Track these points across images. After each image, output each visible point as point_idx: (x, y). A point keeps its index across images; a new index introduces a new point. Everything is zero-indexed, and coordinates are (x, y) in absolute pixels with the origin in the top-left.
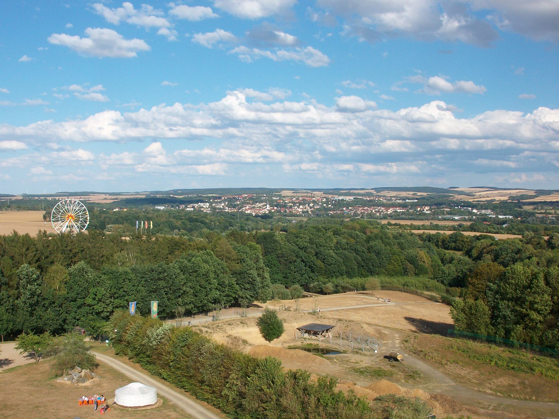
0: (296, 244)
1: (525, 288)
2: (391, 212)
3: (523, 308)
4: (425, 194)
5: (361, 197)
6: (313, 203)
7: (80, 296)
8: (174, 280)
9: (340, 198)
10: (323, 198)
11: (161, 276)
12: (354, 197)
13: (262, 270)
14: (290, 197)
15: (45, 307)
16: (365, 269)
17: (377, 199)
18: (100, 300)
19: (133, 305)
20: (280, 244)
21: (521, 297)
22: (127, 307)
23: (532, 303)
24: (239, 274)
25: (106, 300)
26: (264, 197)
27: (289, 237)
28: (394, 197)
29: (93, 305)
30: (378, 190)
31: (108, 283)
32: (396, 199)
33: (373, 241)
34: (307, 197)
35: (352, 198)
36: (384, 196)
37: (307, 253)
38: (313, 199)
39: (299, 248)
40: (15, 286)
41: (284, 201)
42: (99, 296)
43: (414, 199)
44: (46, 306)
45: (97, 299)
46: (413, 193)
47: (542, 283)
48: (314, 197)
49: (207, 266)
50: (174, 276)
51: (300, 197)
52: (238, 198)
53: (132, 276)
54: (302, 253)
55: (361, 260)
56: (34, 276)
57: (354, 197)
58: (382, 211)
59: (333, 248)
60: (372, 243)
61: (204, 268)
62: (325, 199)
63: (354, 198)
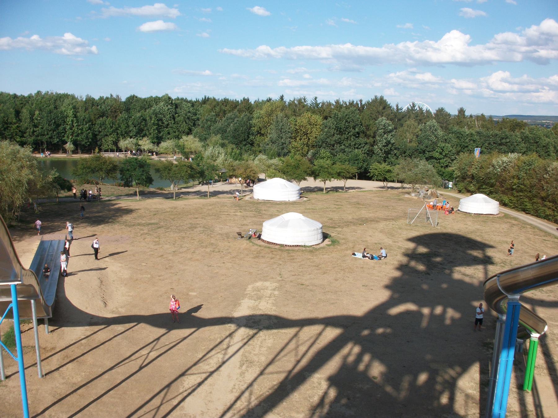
7: (428, 149)
8: (515, 147)
11: (504, 141)
15: (396, 156)
18: (446, 156)
19: (477, 151)
22: (472, 152)
40: (372, 134)
44: (397, 155)
45: (444, 154)
50: (515, 144)
56: (390, 128)
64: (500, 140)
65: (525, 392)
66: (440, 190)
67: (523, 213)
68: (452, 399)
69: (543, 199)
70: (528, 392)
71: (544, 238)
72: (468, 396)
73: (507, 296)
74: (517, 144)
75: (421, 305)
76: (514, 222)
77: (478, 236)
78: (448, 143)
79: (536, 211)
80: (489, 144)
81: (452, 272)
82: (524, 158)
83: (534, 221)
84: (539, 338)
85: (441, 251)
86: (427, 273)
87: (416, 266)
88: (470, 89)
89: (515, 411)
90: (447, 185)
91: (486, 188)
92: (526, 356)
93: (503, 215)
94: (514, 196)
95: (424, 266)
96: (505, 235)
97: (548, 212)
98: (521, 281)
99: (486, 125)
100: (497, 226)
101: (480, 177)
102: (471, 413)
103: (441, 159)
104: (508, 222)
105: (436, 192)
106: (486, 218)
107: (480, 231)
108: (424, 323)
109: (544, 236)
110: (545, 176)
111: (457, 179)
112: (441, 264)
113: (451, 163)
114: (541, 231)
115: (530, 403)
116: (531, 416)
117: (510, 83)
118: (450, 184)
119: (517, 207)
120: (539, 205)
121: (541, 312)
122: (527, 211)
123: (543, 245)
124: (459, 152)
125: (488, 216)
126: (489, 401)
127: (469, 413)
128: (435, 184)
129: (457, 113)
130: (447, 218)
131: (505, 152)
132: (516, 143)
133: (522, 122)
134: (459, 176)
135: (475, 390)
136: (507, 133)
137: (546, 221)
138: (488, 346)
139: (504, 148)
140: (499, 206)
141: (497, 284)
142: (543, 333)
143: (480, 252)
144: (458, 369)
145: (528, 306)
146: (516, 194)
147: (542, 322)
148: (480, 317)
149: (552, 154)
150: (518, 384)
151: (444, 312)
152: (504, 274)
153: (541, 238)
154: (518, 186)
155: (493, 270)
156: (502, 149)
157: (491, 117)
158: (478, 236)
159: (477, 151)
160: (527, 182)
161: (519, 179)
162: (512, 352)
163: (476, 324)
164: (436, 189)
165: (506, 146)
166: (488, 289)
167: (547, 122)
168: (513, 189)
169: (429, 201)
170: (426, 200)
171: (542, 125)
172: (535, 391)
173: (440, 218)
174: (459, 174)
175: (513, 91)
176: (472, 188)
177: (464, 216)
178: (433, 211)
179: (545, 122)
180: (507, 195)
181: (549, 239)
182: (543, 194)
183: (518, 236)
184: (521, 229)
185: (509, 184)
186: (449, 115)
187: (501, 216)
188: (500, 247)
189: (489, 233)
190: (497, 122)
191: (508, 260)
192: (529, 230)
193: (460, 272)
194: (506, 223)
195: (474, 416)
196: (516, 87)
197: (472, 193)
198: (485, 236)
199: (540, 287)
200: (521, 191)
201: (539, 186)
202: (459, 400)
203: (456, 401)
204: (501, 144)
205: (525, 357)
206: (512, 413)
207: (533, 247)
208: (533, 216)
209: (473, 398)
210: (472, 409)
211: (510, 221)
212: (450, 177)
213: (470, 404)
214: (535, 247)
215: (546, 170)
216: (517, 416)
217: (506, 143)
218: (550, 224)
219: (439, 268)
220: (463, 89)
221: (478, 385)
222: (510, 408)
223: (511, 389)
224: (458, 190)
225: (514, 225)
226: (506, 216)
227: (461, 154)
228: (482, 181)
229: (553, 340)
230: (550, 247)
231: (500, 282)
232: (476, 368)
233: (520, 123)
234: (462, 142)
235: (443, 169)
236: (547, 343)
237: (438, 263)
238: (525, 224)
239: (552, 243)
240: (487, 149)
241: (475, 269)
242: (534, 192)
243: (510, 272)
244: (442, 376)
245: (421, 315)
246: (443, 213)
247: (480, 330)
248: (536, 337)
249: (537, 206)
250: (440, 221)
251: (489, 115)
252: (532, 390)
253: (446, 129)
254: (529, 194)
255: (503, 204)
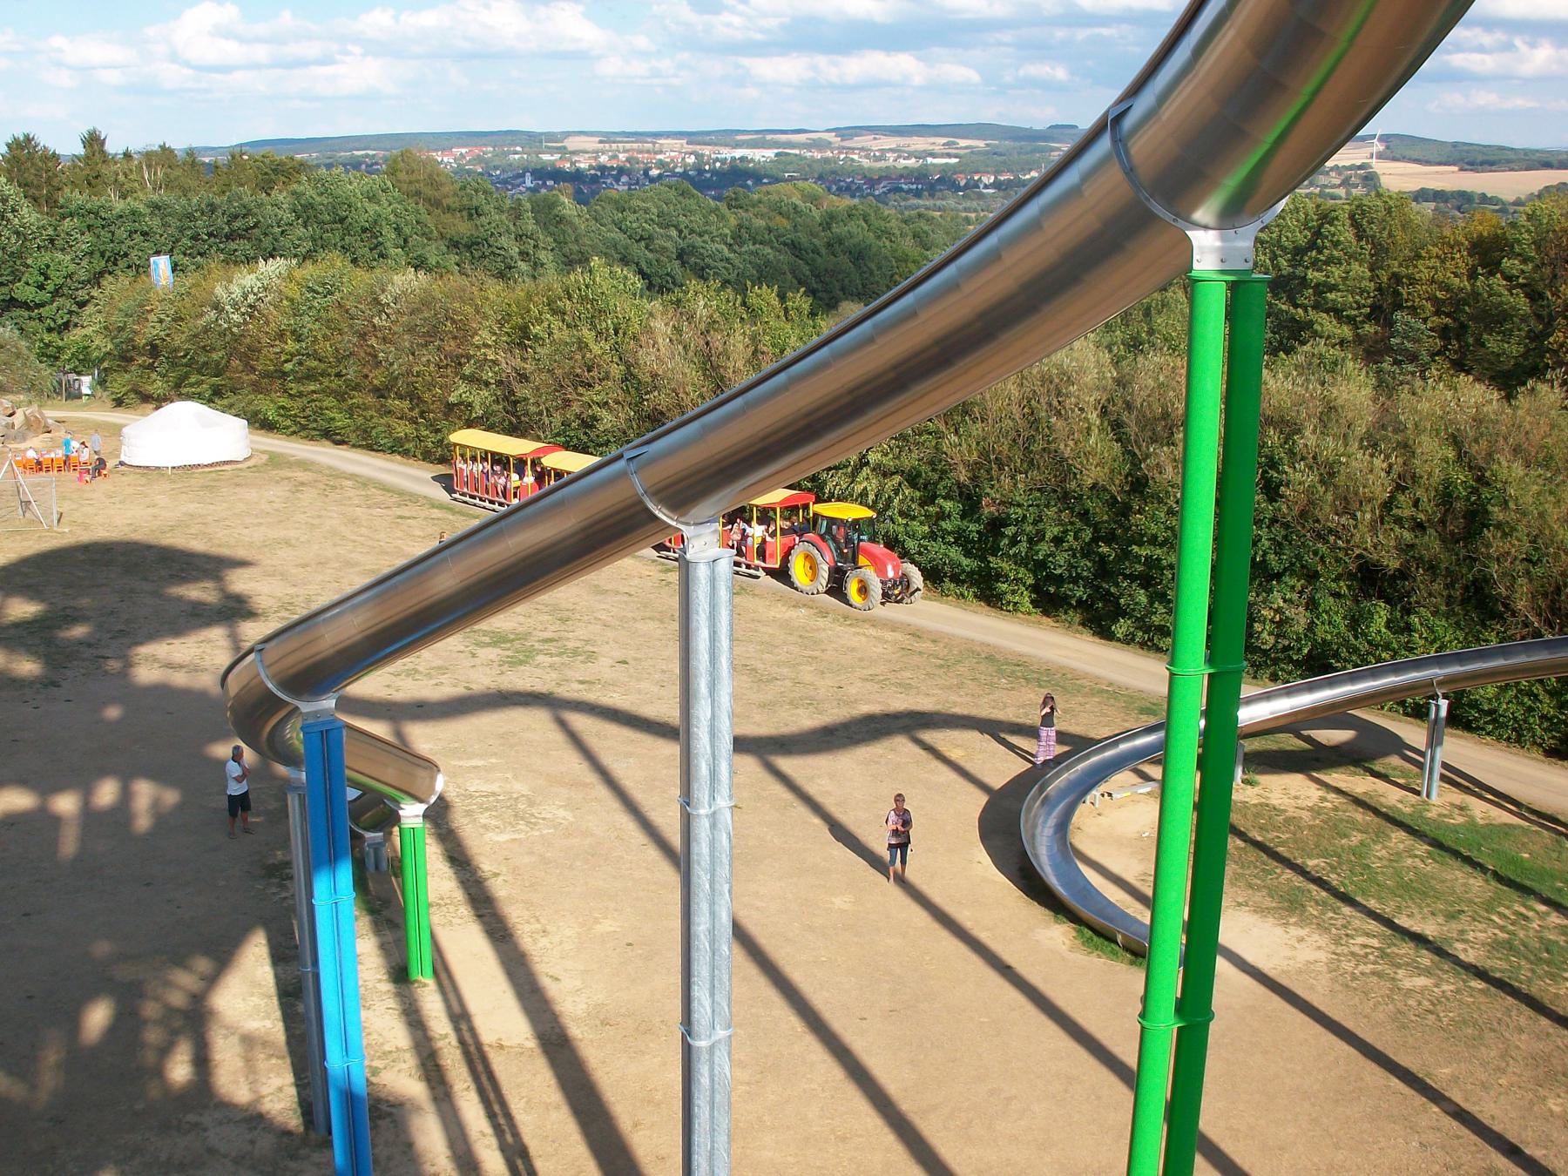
0: (620, 229)
1: (1298, 252)
2: (884, 189)
3: (1296, 306)
4: (981, 144)
5: (797, 152)
6: (659, 168)
9: (738, 153)
10: (686, 153)
11: (237, 224)
12: (776, 151)
13: (532, 242)
14: (593, 152)
16: (821, 299)
17: (842, 157)
20: (575, 229)
21: (1292, 277)
22: (142, 269)
23: (1321, 289)
24: (468, 247)
25: (77, 289)
26: (516, 153)
27: (598, 207)
28: (892, 150)
29: (38, 306)
30: (845, 133)
31: (85, 242)
32: (899, 157)
33: (841, 224)
34: (641, 152)
35: (770, 154)
36: (862, 149)
37: (651, 251)
38: (659, 157)
39: (630, 237)
41: (573, 163)
42: (56, 278)
43: (949, 156)
45: (50, 287)
46: (945, 140)
47: (1347, 235)
48: (661, 152)
49: (372, 208)
50: (277, 230)
51: (619, 152)
52: (440, 159)
53: (155, 223)
54: (638, 250)
55: (808, 273)
57: (776, 151)
58: (858, 187)
59: (729, 240)
60: (837, 229)
61: (367, 212)
62: (693, 157)
63: (777, 155)
64: (228, 223)
65: (416, 985)
66: (54, 408)
67: (327, 443)
68: (202, 1062)
69: (380, 393)
70: (425, 985)
71: (399, 512)
72: (249, 1041)
73: (297, 708)
74: (283, 232)
75: (46, 786)
76: (301, 476)
77: (195, 536)
78: (63, 250)
79: (365, 431)
80: (195, 238)
81: (129, 664)
82: (310, 271)
83: (367, 465)
84: (426, 816)
85: (85, 602)
86: (47, 683)
87: (10, 665)
88: (115, 67)
89: (398, 1049)
90: (77, 386)
91: (199, 383)
92: (400, 879)
93: (265, 457)
94: (290, 395)
95: (34, 662)
96: (281, 521)
97: (402, 429)
98: (331, 651)
99: (177, 178)
100: (251, 494)
101: (176, 350)
102: (270, 1090)
103: (42, 305)
104: (283, 479)
105: (41, 414)
106: (214, 475)
107: (200, 520)
108: (69, 844)
109: (399, 506)
110: (376, 320)
111: (106, 365)
112: (90, 645)
113: (78, 313)
114: (388, 491)
115: (437, 1015)
116: (445, 1050)
117: (241, 40)
118: (86, 383)
119: (304, 428)
120: (370, 413)
121: (424, 737)
122: (338, 434)
123: (399, 534)
124: (101, 274)
125: (218, 468)
126: (315, 1041)
127: (264, 1090)
128: (32, 387)
129: (80, 150)
130: (86, 495)
131: (250, 260)
132: (279, 227)
133: (292, 159)
134: (109, 353)
135: (267, 1017)
136: (246, 200)
137: (398, 457)
138: (279, 873)
139: (242, 246)
140: (250, 433)
141: (259, 675)
142: (433, 799)
143: (210, 585)
144: (203, 964)
145: (379, 729)
146: (294, 388)
147: (426, 768)
148: (236, 789)
149: (393, 251)
150: (392, 968)
151: (126, 796)
152: (273, 643)
153: (389, 512)
154: (300, 364)
155: (252, 632)
156: (236, 250)
157: (191, 152)
158: (195, 536)
159: (161, 266)
160: (325, 348)
161: (299, 339)
162: (345, 874)
163: (233, 813)
164: (40, 406)
165: (249, 239)
166: (237, 695)
167: (367, 156)
168: (285, 374)
169: (22, 446)
170: (10, 446)
171: (355, 165)
172: (443, 976)
173: (64, 498)
174: (110, 346)
175: (257, 66)
176: (157, 386)
177: (144, 481)
178: (42, 477)
179: (362, 156)
180: (267, 392)
181: (414, 514)
182: (378, 377)
183: (319, 517)
184: (327, 496)
185: (271, 360)
186: (55, 157)
187: (260, 462)
188: (269, 561)
189: (227, 523)
190: (214, 167)
191: (297, 596)
192: (352, 493)
193: (156, 660)
194: (277, 482)
195: (281, 1095)
196: (261, 53)
197: (159, 401)
198: (216, 533)
199: (397, 658)
200: (310, 376)
201: (363, 354)
202: (224, 1060)
203: (216, 1066)
204: (230, 237)
205: (398, 882)
206: (390, 1058)
207: (370, 543)
208: (359, 450)
209: (265, 1044)
210: (271, 1075)
211: (290, 475)
212: (84, 362)
213: (262, 1065)
214: (375, 544)
215: (377, 301)
216: (405, 1062)
217: (246, 230)
218: (411, 466)
219: (84, 660)
220: (94, 68)
221: (275, 1001)
222: (383, 1044)
223: (375, 987)
224: (114, 400)
225: (302, 484)
226: (275, 461)
227: (107, 281)
228: (184, 361)
229: (469, 813)
230: (419, 537)
231: (269, 666)
232: (257, 949)
233: (284, 164)
234: (104, 243)
235: (54, 337)
236: (454, 825)
237: (80, 643)
238: (337, 477)
239: (425, 523)
240: (190, 254)
241: (201, 642)
242: (351, 373)
243: (286, 635)
244: (157, 999)
245: (56, 821)
246: (73, 482)
247: (246, 831)
248: (417, 816)
249: (365, 418)
250: (66, 507)
251: (185, 146)
252: (435, 972)
253: (47, 200)
254: (336, 384)
255: (262, 424)
